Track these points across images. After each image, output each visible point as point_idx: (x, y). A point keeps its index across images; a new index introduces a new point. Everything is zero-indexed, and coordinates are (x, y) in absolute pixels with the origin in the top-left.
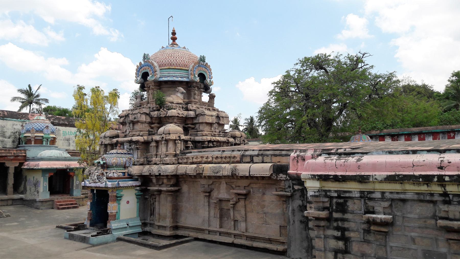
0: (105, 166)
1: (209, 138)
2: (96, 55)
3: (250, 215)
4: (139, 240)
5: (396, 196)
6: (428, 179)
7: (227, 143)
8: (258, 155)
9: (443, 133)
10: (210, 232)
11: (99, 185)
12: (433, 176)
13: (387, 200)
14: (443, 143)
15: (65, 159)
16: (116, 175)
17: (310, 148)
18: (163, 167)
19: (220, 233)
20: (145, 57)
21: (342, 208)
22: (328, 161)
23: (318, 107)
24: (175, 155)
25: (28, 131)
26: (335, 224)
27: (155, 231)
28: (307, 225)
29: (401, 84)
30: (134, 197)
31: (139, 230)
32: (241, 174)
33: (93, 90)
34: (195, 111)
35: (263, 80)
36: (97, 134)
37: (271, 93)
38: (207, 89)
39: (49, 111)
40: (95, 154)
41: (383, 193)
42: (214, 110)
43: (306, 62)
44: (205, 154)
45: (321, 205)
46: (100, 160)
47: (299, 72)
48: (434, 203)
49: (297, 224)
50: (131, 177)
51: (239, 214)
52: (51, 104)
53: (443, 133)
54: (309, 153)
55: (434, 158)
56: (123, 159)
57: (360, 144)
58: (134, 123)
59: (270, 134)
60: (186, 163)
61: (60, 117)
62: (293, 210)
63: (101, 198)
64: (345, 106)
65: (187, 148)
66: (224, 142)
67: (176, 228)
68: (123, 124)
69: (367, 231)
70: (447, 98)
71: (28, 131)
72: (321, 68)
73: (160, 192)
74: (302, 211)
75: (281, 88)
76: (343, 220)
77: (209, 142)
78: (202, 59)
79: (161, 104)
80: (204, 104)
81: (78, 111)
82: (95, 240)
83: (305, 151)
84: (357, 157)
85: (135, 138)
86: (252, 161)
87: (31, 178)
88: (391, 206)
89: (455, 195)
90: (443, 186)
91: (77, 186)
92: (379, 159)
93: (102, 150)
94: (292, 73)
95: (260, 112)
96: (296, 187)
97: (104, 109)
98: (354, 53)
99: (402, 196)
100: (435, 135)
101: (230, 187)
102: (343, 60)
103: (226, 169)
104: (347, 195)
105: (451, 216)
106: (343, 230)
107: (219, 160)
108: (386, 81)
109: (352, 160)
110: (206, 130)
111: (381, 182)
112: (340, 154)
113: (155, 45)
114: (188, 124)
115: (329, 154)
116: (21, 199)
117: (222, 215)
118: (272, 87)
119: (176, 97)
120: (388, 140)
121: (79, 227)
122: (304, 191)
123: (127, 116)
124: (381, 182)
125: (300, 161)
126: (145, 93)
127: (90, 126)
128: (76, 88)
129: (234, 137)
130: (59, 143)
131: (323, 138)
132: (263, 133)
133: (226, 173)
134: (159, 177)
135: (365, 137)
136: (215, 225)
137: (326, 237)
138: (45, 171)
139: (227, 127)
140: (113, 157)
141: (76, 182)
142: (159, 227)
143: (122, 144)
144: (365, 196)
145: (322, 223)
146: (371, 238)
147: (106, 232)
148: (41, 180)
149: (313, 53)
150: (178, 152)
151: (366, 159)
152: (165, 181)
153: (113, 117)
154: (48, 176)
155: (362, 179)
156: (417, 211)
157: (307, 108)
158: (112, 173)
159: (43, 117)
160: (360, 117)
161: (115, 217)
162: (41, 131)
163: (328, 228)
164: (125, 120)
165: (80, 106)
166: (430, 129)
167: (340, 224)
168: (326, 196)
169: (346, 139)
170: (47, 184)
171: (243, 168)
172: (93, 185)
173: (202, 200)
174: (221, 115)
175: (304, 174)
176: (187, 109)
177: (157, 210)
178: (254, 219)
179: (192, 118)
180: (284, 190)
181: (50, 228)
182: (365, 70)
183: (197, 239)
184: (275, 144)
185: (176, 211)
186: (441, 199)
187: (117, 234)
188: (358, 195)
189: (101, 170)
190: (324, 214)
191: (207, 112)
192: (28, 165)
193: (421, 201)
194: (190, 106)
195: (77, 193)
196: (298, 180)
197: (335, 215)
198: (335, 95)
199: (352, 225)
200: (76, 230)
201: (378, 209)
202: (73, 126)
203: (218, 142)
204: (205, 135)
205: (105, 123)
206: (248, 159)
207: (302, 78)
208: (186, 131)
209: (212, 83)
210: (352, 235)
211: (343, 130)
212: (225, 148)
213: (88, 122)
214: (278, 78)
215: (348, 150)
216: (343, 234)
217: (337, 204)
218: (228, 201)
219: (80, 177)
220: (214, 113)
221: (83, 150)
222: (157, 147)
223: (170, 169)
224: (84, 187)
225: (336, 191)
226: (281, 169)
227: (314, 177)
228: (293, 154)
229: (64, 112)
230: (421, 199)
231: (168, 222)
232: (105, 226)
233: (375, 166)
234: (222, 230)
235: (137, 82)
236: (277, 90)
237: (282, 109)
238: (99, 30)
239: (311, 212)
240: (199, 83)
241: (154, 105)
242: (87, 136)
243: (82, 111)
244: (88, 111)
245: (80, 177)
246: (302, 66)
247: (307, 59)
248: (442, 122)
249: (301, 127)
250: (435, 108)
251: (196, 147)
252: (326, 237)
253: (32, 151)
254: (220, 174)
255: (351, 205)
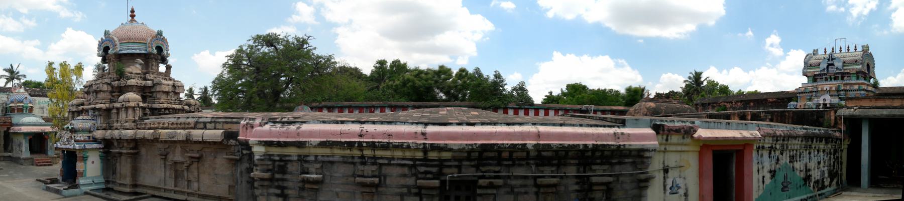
0: (73, 131)
1: (165, 106)
2: (63, 35)
3: (202, 177)
4: (103, 195)
5: (326, 159)
6: (350, 145)
7: (183, 111)
8: (210, 122)
9: (367, 107)
10: (165, 190)
11: (68, 146)
12: (355, 142)
13: (319, 162)
14: (365, 116)
15: (41, 125)
16: (82, 139)
17: (258, 117)
18: (124, 132)
19: (175, 192)
20: (106, 33)
21: (283, 170)
22: (273, 129)
23: (267, 80)
24: (135, 121)
25: (12, 102)
26: (276, 184)
27: (117, 188)
28: (253, 185)
29: (338, 65)
30: (98, 158)
31: (103, 186)
32: (195, 139)
33: (61, 65)
34: (152, 80)
35: (218, 53)
36: (66, 102)
37: (224, 65)
38: (164, 60)
39: (27, 84)
40: (65, 120)
41: (316, 156)
42: (171, 80)
43: (258, 38)
44: (162, 121)
45: (265, 167)
46: (68, 125)
47: (251, 47)
48: (354, 164)
49: (244, 183)
50: (95, 140)
51: (193, 175)
52: (28, 79)
53: (367, 107)
54: (258, 121)
55: (356, 128)
56: (88, 125)
57: (301, 114)
58: (97, 92)
59: (223, 103)
60: (144, 129)
61: (36, 89)
62: (241, 172)
63: (70, 158)
64: (290, 81)
65: (145, 114)
66: (179, 110)
67: (135, 186)
68: (88, 93)
69: (302, 189)
70: (372, 80)
71: (12, 102)
72: (272, 45)
73: (121, 154)
74: (249, 173)
75: (234, 61)
76: (283, 180)
77: (166, 109)
78: (160, 33)
79: (121, 75)
80: (161, 74)
81: (50, 83)
82: (66, 193)
83: (254, 119)
84: (297, 125)
85: (98, 106)
86: (205, 128)
87: (16, 140)
88: (322, 167)
89: (369, 158)
90: (362, 150)
91: (51, 148)
92: (315, 127)
93: (70, 116)
94: (244, 48)
95: (213, 82)
96: (245, 152)
97: (71, 80)
98: (301, 35)
99: (331, 159)
100: (361, 109)
101: (184, 150)
102: (291, 40)
103: (181, 134)
104: (287, 158)
105: (366, 174)
106: (283, 188)
107: (175, 126)
108: (326, 62)
109: (293, 128)
110: (163, 98)
111: (315, 147)
112: (283, 123)
113: (116, 21)
114: (146, 93)
115: (275, 122)
116: (10, 156)
117: (177, 176)
118: (225, 60)
119: (135, 68)
120: (325, 112)
121: (54, 181)
122: (251, 155)
123: (91, 86)
124: (315, 147)
125: (249, 129)
126: (106, 65)
127: (60, 96)
128: (47, 64)
129: (189, 105)
130: (35, 111)
131: (270, 108)
132: (216, 102)
133: (181, 138)
134: (120, 140)
135: (306, 108)
136: (170, 185)
137: (269, 195)
138: (26, 134)
139: (182, 96)
140: (80, 123)
141: (50, 144)
142: (120, 185)
143: (87, 111)
144: (302, 159)
145: (266, 183)
146: (305, 194)
147: (75, 186)
148: (23, 141)
149: (265, 32)
150: (137, 118)
151: (305, 127)
152: (125, 144)
153: (78, 87)
154: (28, 138)
155: (300, 145)
156: (341, 171)
157: (258, 80)
158: (79, 137)
159: (22, 90)
160: (303, 90)
161: (82, 174)
162: (22, 102)
163: (270, 187)
164: (89, 89)
165: (51, 79)
166: (357, 103)
167: (280, 183)
168: (270, 160)
169: (291, 110)
170: (27, 145)
171: (197, 134)
172: (63, 146)
173: (159, 162)
174: (177, 84)
175: (252, 140)
176: (145, 79)
177: (118, 170)
178: (206, 180)
179: (150, 87)
180: (233, 154)
181: (32, 180)
182: (309, 51)
183: (154, 196)
184: (227, 112)
185: (135, 172)
186: (359, 160)
187: (84, 189)
188: (296, 158)
189: (69, 134)
190: (267, 175)
191: (164, 82)
192: (15, 129)
193: (345, 163)
194: (148, 76)
195: (51, 153)
196: (246, 145)
197: (277, 176)
198: (282, 70)
199: (290, 184)
200: (51, 183)
201: (312, 169)
202: (46, 96)
203: (174, 109)
204: (163, 103)
205: (72, 93)
206: (202, 126)
207: (254, 53)
208: (144, 99)
209: (168, 55)
210: (290, 192)
211: (288, 101)
212: (180, 115)
213: (58, 92)
214: (232, 52)
215: (291, 119)
216: (283, 192)
217: (280, 166)
218: (183, 163)
219: (53, 140)
220: (171, 83)
221: (54, 117)
222: (118, 113)
223: (129, 133)
224: (57, 149)
225: (278, 155)
226: (231, 135)
227: (260, 143)
228: (242, 122)
229: (38, 85)
230: (345, 161)
231: (128, 181)
232: (75, 181)
233: (311, 134)
234: (177, 189)
235: (99, 55)
236: (231, 63)
237: (234, 81)
238: (65, 14)
239: (257, 173)
240: (156, 54)
241: (114, 76)
242: (57, 104)
243: (52, 83)
244: (58, 82)
245: (53, 140)
246: (255, 42)
247: (259, 37)
248: (366, 99)
249: (251, 98)
250: (362, 87)
251: (153, 114)
252: (269, 195)
253: (16, 118)
254: (175, 139)
255: (291, 167)
